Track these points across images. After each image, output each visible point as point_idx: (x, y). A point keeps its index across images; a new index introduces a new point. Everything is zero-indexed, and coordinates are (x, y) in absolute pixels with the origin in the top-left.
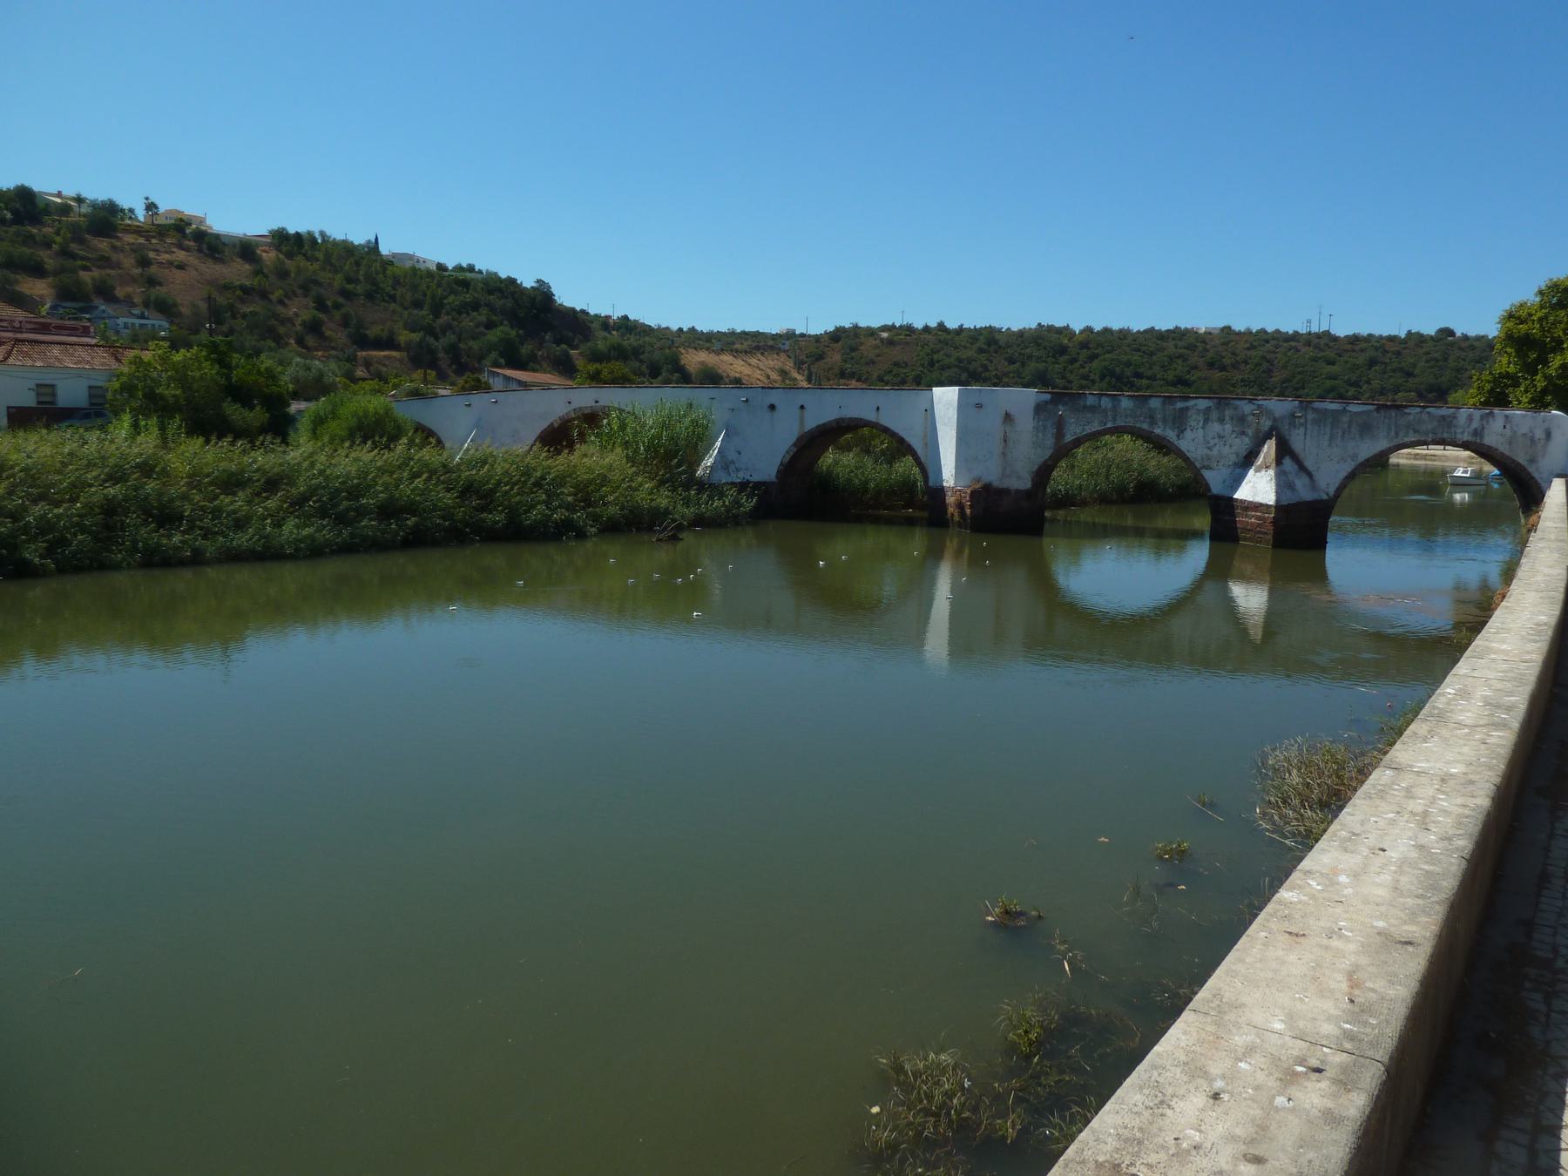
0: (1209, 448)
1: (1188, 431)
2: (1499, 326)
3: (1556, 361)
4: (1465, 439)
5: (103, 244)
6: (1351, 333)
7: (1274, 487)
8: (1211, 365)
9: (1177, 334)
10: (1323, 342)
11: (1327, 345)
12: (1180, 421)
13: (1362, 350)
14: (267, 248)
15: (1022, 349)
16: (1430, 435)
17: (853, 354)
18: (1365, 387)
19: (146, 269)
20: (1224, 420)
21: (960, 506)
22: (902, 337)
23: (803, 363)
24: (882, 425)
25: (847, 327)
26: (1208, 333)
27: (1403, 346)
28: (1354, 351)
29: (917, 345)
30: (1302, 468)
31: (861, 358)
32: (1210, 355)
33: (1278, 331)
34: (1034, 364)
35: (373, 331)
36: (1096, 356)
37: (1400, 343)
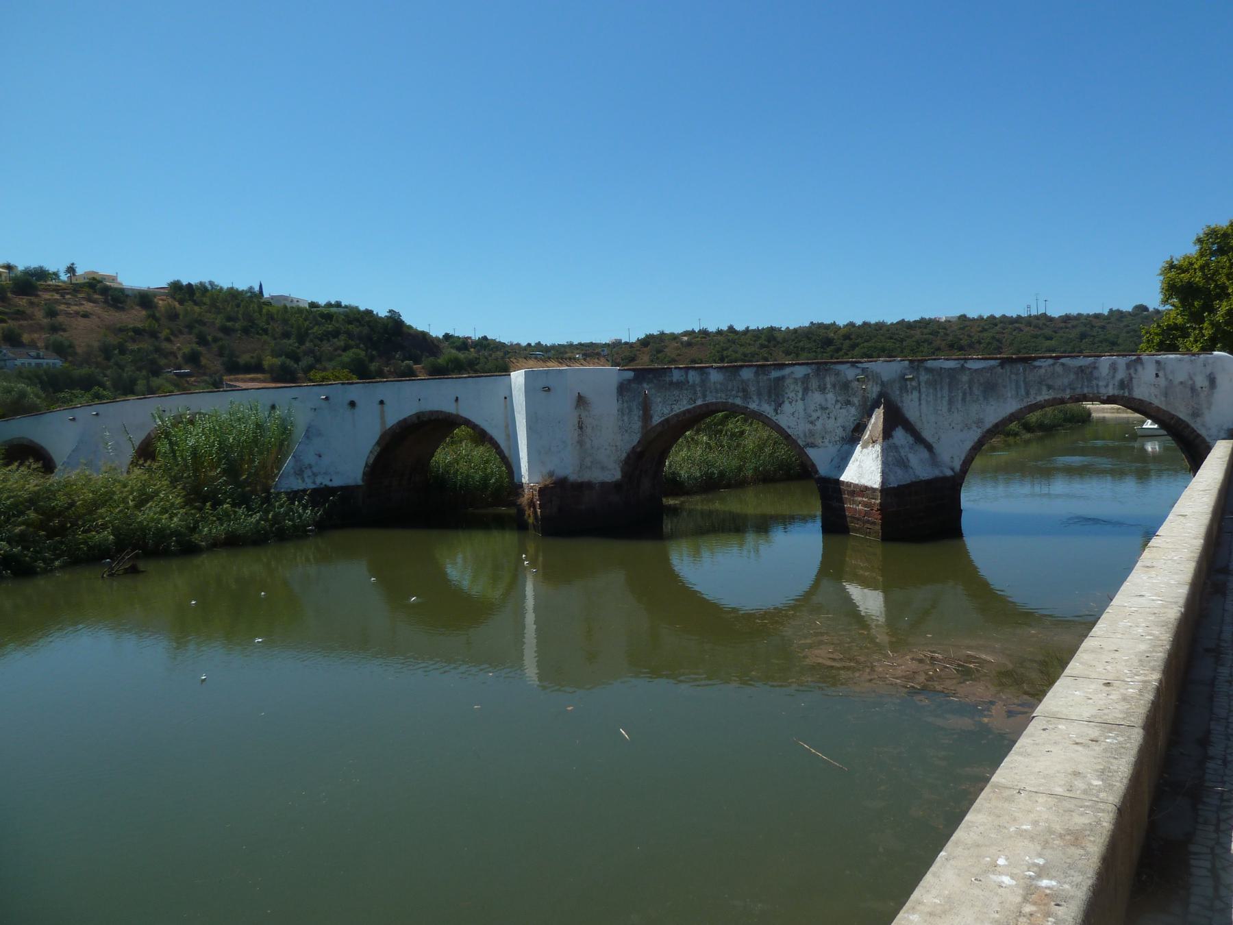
0: (812, 423)
2: (1161, 278)
3: (1223, 308)
5: (22, 302)
7: (880, 466)
9: (923, 324)
11: (1045, 324)
12: (776, 393)
13: (1074, 327)
14: (165, 297)
15: (796, 343)
16: (1068, 391)
17: (659, 355)
20: (825, 389)
22: (699, 339)
24: (462, 417)
26: (948, 321)
27: (1108, 321)
29: (710, 345)
30: (918, 439)
31: (665, 358)
32: (950, 338)
33: (1004, 316)
35: (244, 359)
36: (857, 345)
37: (1104, 319)
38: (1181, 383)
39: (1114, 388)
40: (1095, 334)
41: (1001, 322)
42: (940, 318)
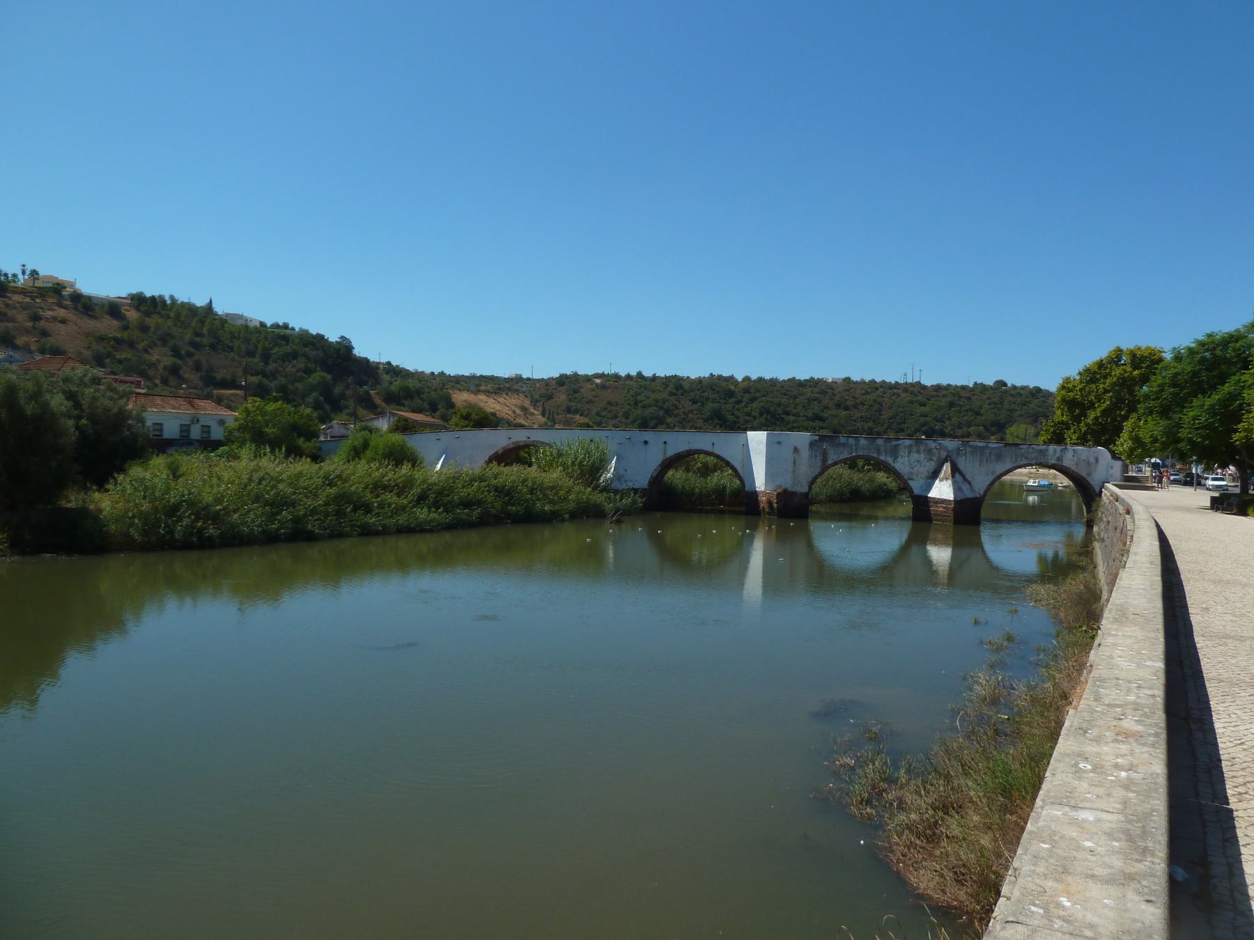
1: (900, 458)
6: (935, 383)
8: (838, 406)
9: (813, 383)
10: (915, 391)
11: (919, 392)
12: (894, 452)
13: (943, 396)
17: (576, 395)
18: (947, 422)
19: (37, 323)
21: (770, 503)
23: (537, 401)
25: (568, 374)
26: (834, 382)
28: (938, 396)
29: (624, 389)
30: (965, 479)
31: (582, 398)
32: (837, 398)
34: (711, 404)
35: (220, 375)
37: (970, 391)
40: (962, 403)
41: (882, 387)
42: (827, 379)
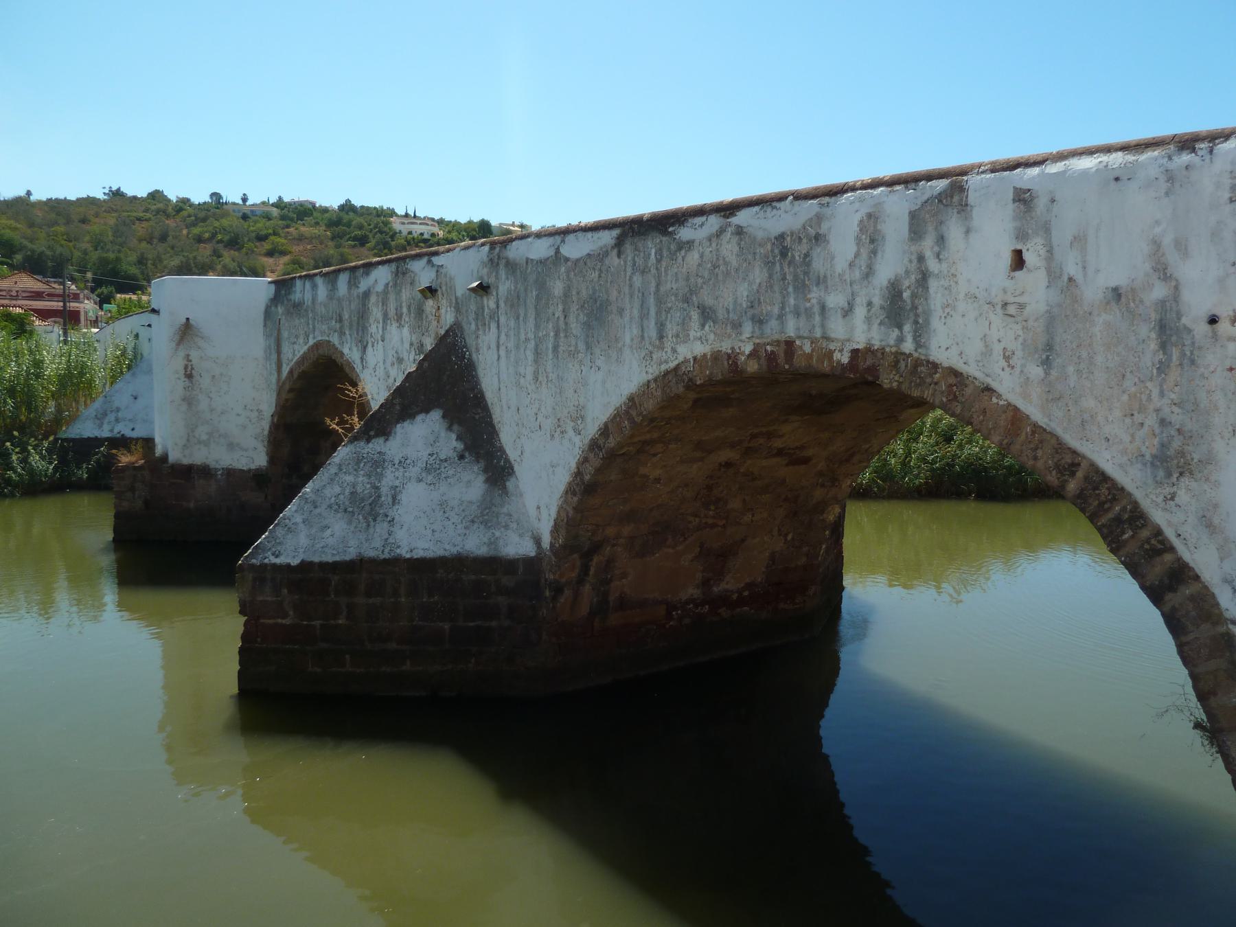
4: (860, 342)
16: (748, 329)
38: (1117, 294)
39: (868, 320)
